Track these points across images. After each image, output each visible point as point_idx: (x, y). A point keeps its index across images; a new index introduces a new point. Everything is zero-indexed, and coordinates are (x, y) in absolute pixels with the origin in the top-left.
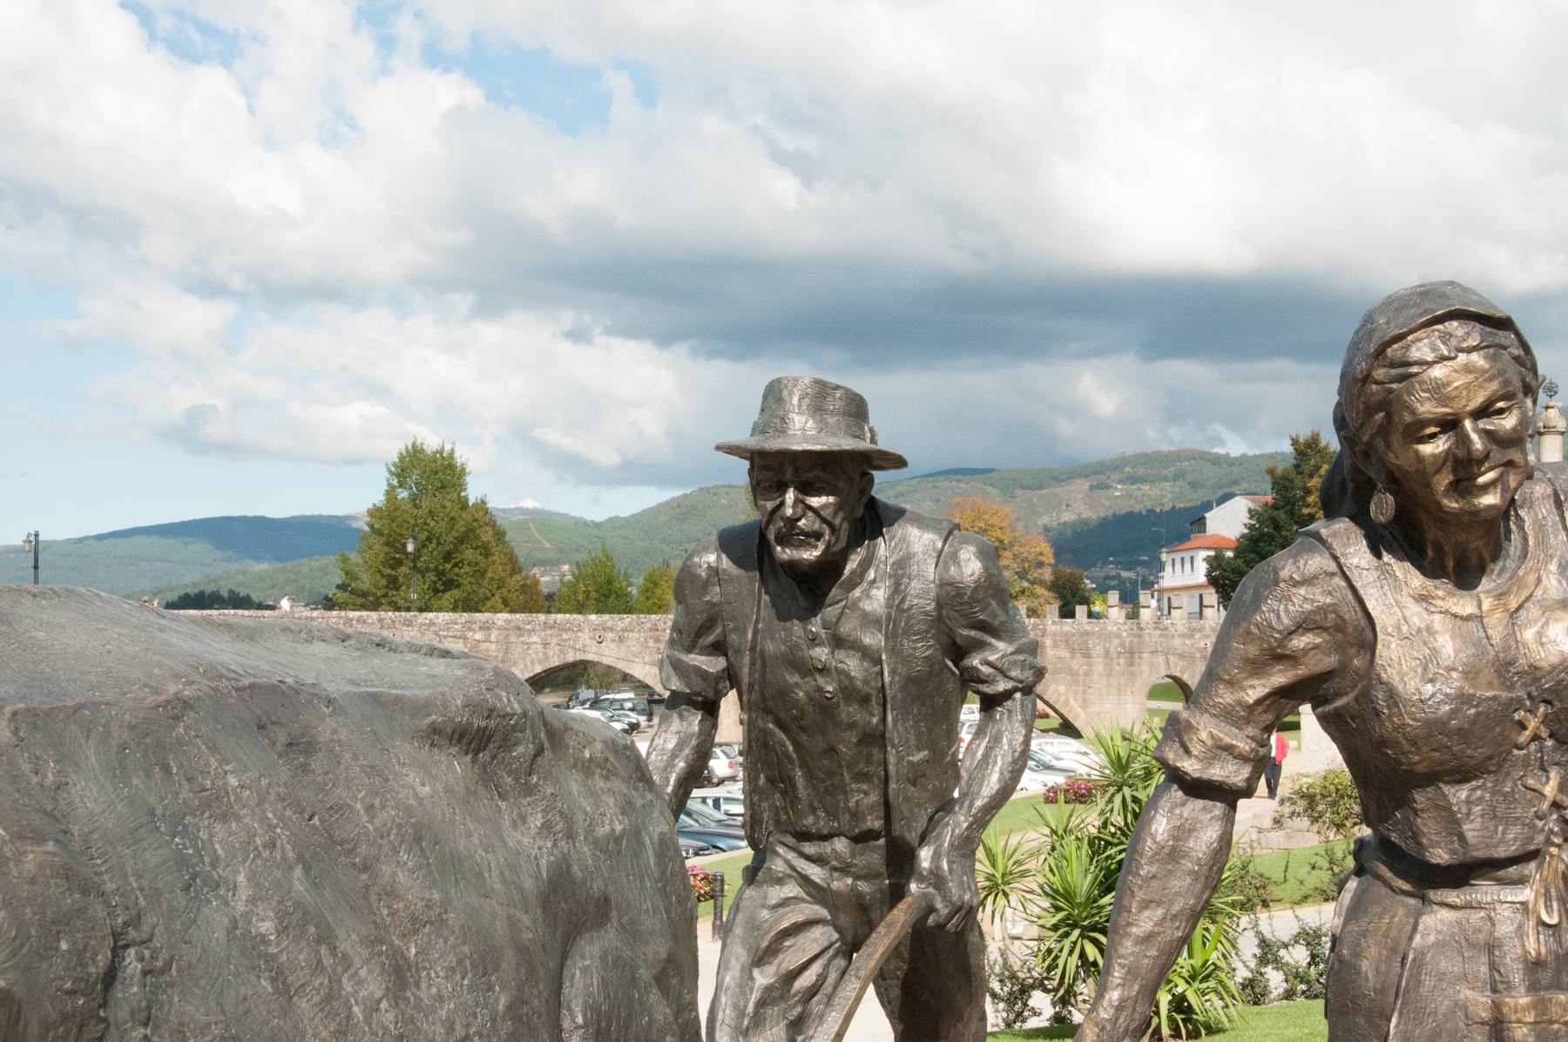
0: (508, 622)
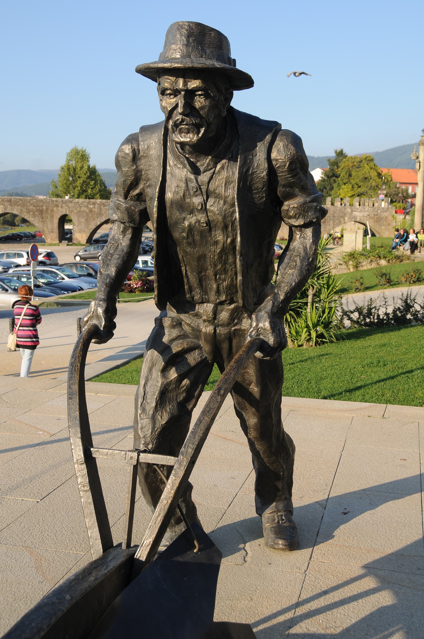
0: (100, 202)
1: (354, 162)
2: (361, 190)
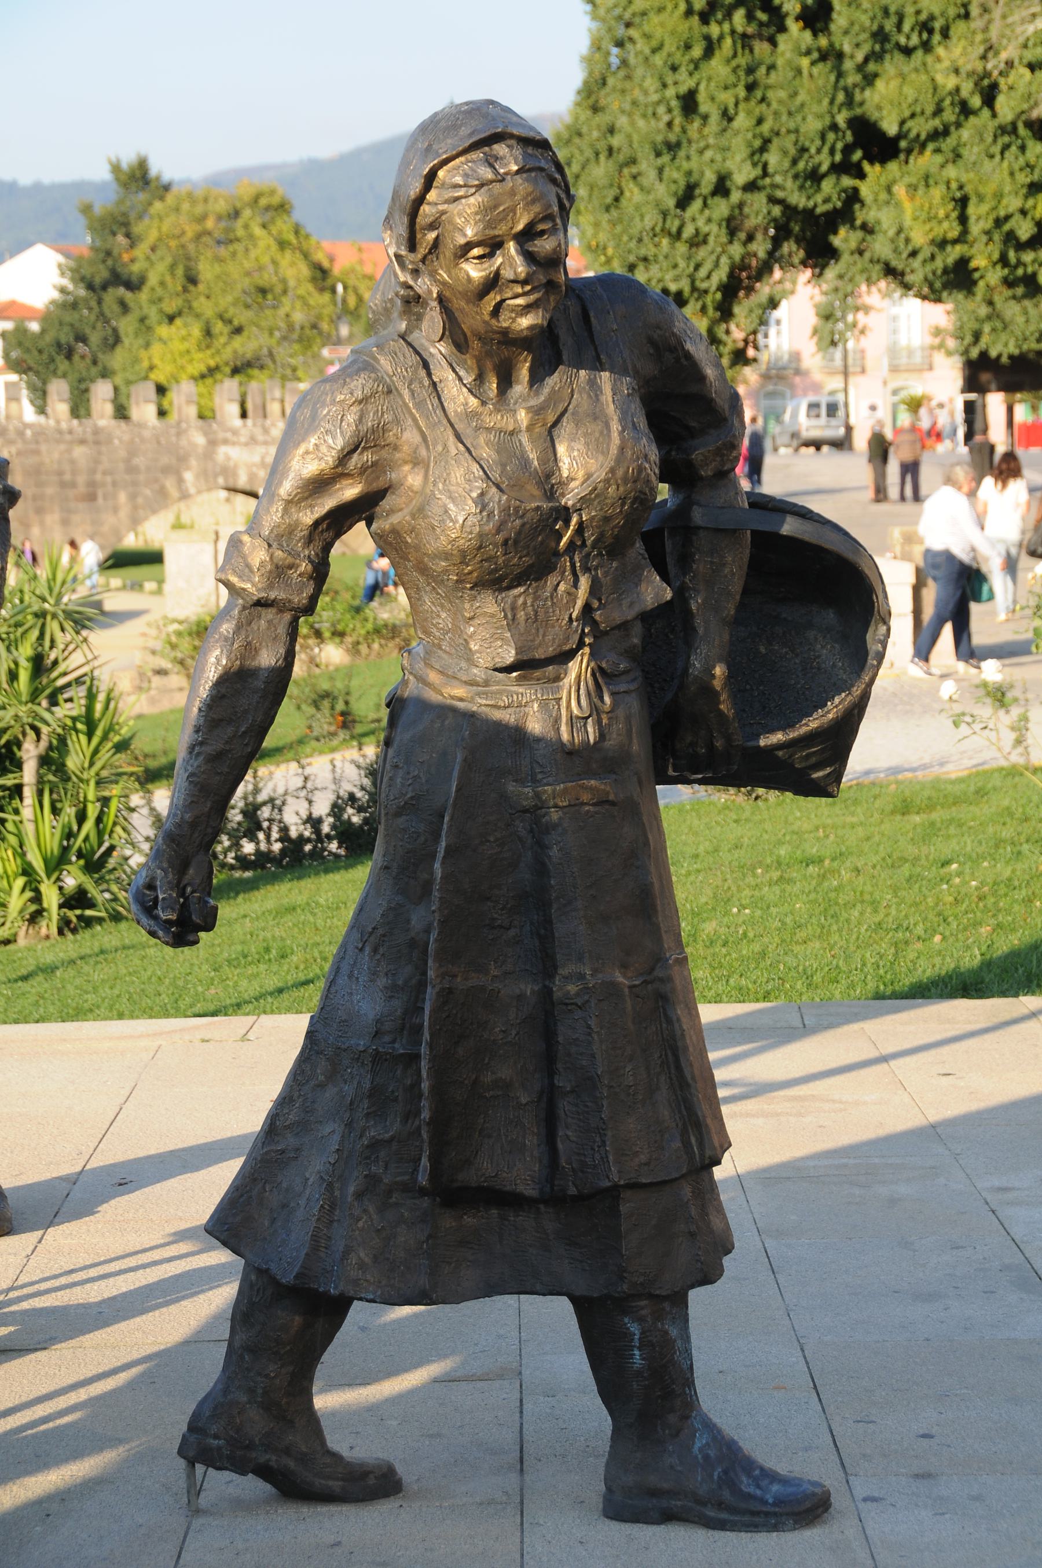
1: (202, 219)
2: (244, 346)
